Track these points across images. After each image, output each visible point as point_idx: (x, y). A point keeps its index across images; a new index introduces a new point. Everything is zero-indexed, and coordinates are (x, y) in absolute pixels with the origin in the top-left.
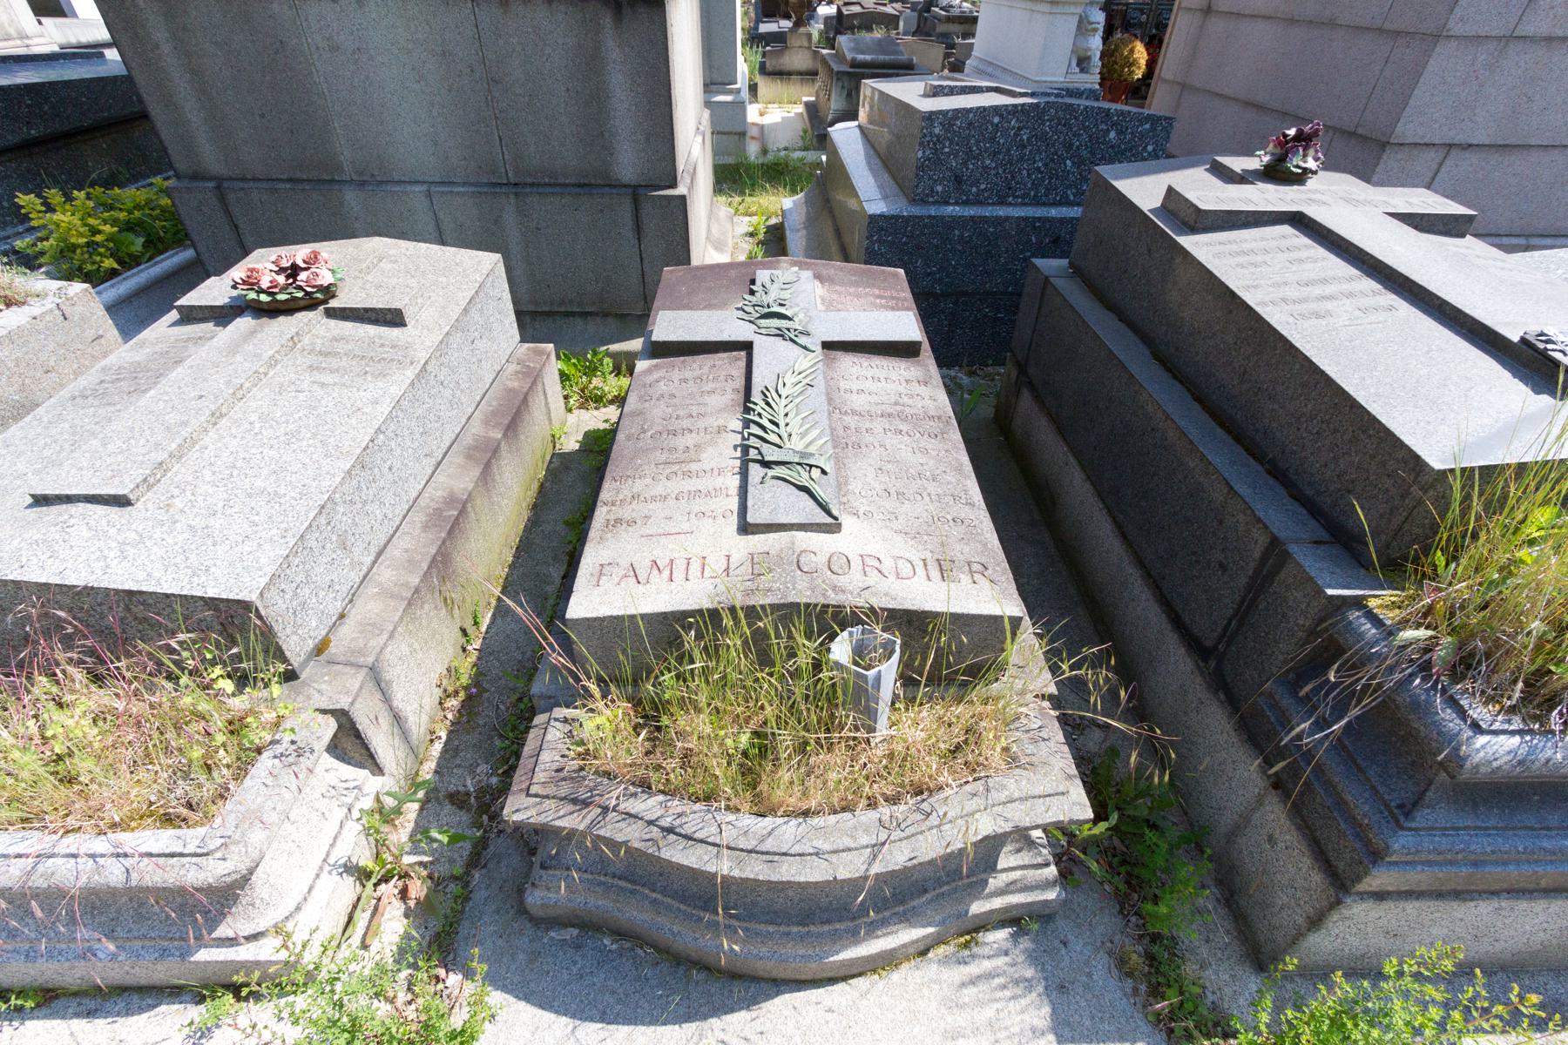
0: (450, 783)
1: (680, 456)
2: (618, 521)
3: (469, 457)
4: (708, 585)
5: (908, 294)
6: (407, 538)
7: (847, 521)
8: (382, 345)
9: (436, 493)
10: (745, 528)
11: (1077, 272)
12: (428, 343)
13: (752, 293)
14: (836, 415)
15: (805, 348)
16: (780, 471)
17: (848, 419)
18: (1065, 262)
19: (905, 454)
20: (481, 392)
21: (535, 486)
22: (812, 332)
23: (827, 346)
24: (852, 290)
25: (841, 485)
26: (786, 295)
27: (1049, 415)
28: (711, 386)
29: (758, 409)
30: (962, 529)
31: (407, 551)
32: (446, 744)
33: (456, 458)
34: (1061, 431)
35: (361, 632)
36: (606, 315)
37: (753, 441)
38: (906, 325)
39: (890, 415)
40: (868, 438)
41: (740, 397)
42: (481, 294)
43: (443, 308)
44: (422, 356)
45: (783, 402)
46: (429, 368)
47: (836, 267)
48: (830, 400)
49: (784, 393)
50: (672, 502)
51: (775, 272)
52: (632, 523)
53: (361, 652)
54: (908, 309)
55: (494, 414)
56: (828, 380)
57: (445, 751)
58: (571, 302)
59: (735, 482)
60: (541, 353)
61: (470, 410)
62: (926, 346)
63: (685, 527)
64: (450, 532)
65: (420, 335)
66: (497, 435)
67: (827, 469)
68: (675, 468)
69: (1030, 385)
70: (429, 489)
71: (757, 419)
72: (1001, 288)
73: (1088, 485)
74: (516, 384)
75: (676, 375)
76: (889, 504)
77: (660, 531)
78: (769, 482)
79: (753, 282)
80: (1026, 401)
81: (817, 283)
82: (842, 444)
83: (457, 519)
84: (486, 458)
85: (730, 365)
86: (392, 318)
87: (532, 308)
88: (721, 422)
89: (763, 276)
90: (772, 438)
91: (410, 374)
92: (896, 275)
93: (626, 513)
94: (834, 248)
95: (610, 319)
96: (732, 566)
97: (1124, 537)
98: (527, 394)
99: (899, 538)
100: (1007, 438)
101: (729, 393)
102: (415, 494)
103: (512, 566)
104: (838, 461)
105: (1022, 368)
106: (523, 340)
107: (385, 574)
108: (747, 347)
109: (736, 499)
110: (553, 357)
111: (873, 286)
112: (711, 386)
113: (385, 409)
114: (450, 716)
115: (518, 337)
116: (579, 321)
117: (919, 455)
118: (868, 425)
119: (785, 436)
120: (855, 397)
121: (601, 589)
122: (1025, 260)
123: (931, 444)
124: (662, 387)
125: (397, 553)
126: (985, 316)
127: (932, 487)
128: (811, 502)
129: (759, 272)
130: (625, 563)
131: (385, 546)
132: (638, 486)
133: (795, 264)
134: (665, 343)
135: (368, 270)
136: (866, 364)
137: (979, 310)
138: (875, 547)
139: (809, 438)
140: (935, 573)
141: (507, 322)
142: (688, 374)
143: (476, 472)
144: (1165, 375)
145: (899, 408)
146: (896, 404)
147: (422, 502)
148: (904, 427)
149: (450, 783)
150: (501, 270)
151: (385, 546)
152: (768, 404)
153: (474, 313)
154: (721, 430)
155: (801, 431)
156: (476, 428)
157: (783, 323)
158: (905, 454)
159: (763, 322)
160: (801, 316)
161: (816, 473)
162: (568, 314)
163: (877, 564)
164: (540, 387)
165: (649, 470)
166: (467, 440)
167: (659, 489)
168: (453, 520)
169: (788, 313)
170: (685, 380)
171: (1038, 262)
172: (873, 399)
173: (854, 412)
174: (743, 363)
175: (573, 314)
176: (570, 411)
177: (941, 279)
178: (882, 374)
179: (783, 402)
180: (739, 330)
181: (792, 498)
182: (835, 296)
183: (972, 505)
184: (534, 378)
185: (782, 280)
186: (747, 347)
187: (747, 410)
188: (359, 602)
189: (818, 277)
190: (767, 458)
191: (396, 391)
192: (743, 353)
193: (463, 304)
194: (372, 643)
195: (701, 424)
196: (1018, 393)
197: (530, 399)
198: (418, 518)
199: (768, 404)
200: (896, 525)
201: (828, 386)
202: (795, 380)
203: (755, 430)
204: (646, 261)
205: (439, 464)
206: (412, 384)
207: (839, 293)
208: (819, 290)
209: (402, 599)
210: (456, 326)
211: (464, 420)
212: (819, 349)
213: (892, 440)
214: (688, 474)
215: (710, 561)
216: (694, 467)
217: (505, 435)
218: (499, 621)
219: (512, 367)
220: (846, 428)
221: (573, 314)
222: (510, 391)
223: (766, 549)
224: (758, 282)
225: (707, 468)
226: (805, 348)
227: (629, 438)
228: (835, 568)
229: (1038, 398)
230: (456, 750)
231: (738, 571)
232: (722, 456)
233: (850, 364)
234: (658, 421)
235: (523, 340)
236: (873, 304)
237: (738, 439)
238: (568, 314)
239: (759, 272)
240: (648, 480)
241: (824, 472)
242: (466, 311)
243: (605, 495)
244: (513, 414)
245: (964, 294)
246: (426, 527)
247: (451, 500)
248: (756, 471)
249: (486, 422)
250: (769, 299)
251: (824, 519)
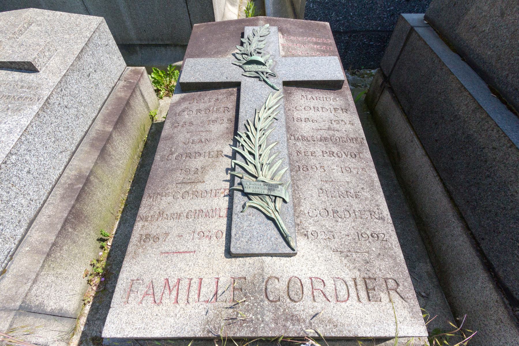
0: (93, 330)
1: (193, 177)
2: (148, 236)
3: (92, 145)
4: (202, 308)
5: (331, 41)
6: (51, 207)
7: (301, 244)
8: (22, 87)
9: (71, 172)
10: (229, 254)
11: (431, 23)
12: (51, 84)
13: (242, 44)
14: (292, 142)
15: (273, 87)
16: (256, 201)
17: (299, 144)
18: (422, 16)
19: (337, 174)
20: (101, 103)
21: (141, 146)
22: (277, 74)
23: (286, 84)
24: (300, 39)
25: (297, 214)
26: (261, 45)
27: (403, 110)
28: (214, 116)
29: (241, 140)
30: (378, 244)
31: (49, 216)
32: (92, 305)
33: (85, 147)
34: (409, 121)
35: (15, 283)
36: (176, 46)
37: (238, 169)
38: (332, 68)
39: (326, 139)
40: (313, 161)
41: (232, 126)
42: (91, 45)
43: (64, 57)
44: (46, 93)
45: (259, 134)
46: (51, 101)
47: (290, 22)
48: (288, 128)
49: (259, 126)
50: (183, 220)
51: (256, 28)
52: (156, 239)
53: (13, 299)
54: (332, 54)
55: (109, 115)
56: (287, 111)
57: (91, 310)
58: (157, 39)
59: (224, 203)
60: (136, 73)
61: (94, 115)
62: (346, 82)
63: (190, 246)
64: (77, 200)
65: (46, 79)
66: (110, 129)
67: (287, 200)
68: (188, 188)
69: (392, 90)
70: (67, 170)
71: (241, 151)
72: (375, 27)
73: (426, 159)
74: (122, 94)
75: (195, 106)
76: (328, 223)
77: (174, 249)
78: (248, 210)
79: (243, 36)
80: (386, 98)
81: (280, 35)
82: (298, 167)
83: (83, 188)
84: (103, 147)
85: (224, 99)
86: (28, 68)
87: (139, 43)
88: (219, 147)
89: (248, 31)
90: (250, 168)
91: (36, 108)
92: (325, 27)
93: (153, 229)
94: (290, 10)
95: (178, 48)
96: (220, 292)
97: (451, 198)
98: (129, 100)
99: (336, 257)
100: (372, 113)
101: (221, 126)
102: (56, 177)
103: (130, 192)
104: (295, 187)
105: (386, 79)
106: (128, 65)
107: (35, 235)
108: (237, 85)
109: (226, 219)
110: (145, 73)
111: (312, 35)
112: (215, 115)
113: (15, 137)
114: (95, 288)
115: (125, 64)
116: (163, 49)
117: (346, 174)
118: (312, 149)
119: (259, 166)
120: (303, 124)
121: (129, 306)
122: (399, 14)
123: (352, 163)
124: (186, 116)
125: (43, 219)
126: (364, 43)
127: (356, 205)
128: (275, 232)
129: (246, 28)
130: (147, 281)
131: (36, 216)
132: (164, 202)
133: (267, 21)
134: (187, 83)
135: (21, 32)
136: (309, 96)
137: (361, 41)
138: (320, 270)
139: (275, 168)
140: (363, 294)
141: (115, 58)
142: (202, 106)
143: (96, 154)
144: (503, 107)
145: (331, 133)
146: (329, 129)
147: (62, 180)
148: (335, 150)
149: (93, 330)
150: (105, 27)
151: (36, 216)
152: (248, 136)
153: (87, 58)
154: (219, 154)
155: (270, 164)
156: (98, 126)
157: (259, 68)
158: (337, 174)
159: (248, 67)
160: (271, 61)
161: (279, 201)
162: (156, 45)
163: (321, 287)
164: (138, 93)
165: (172, 188)
166: (93, 134)
167: (176, 208)
168: (82, 189)
169: (262, 60)
170: (199, 111)
171: (406, 16)
172: (315, 125)
173: (304, 139)
174: (234, 98)
175: (160, 45)
176: (161, 98)
177: (344, 24)
178: (318, 104)
179: (259, 134)
180: (233, 74)
181: (263, 228)
182: (290, 44)
183: (382, 219)
184: (133, 88)
185: (260, 34)
186: (237, 85)
187: (236, 142)
188: (16, 258)
189: (280, 30)
190: (247, 190)
191: (25, 122)
192: (235, 89)
193: (77, 53)
194: (21, 290)
195: (207, 149)
196: (382, 92)
197: (132, 103)
198: (59, 191)
199: (248, 136)
200: (333, 244)
201: (287, 117)
202: (266, 115)
203: (239, 161)
204: (191, 16)
205: (74, 153)
206: (38, 115)
207: (292, 42)
208: (281, 40)
209: (43, 254)
210: (72, 69)
211: (90, 122)
212: (280, 87)
213: (329, 162)
214: (196, 194)
215: (205, 281)
216: (200, 187)
217: (115, 128)
218: (122, 226)
219: (122, 83)
220: (298, 152)
221: (160, 45)
222: (119, 99)
223: (243, 274)
224: (246, 36)
225: (209, 190)
226: (273, 87)
227: (162, 158)
228: (292, 294)
229: (396, 99)
230: (97, 309)
231: (223, 298)
232: (217, 179)
233: (302, 98)
234: (181, 145)
235: (128, 65)
236: (313, 49)
237: (228, 163)
238: (156, 45)
239: (246, 28)
240: (170, 199)
241: (284, 201)
242: (79, 58)
243: (142, 211)
244: (120, 115)
245: (355, 31)
246: (63, 198)
247: (79, 178)
248: (238, 195)
249: (104, 121)
250: (251, 49)
251: (288, 250)
